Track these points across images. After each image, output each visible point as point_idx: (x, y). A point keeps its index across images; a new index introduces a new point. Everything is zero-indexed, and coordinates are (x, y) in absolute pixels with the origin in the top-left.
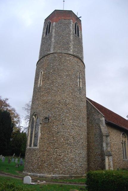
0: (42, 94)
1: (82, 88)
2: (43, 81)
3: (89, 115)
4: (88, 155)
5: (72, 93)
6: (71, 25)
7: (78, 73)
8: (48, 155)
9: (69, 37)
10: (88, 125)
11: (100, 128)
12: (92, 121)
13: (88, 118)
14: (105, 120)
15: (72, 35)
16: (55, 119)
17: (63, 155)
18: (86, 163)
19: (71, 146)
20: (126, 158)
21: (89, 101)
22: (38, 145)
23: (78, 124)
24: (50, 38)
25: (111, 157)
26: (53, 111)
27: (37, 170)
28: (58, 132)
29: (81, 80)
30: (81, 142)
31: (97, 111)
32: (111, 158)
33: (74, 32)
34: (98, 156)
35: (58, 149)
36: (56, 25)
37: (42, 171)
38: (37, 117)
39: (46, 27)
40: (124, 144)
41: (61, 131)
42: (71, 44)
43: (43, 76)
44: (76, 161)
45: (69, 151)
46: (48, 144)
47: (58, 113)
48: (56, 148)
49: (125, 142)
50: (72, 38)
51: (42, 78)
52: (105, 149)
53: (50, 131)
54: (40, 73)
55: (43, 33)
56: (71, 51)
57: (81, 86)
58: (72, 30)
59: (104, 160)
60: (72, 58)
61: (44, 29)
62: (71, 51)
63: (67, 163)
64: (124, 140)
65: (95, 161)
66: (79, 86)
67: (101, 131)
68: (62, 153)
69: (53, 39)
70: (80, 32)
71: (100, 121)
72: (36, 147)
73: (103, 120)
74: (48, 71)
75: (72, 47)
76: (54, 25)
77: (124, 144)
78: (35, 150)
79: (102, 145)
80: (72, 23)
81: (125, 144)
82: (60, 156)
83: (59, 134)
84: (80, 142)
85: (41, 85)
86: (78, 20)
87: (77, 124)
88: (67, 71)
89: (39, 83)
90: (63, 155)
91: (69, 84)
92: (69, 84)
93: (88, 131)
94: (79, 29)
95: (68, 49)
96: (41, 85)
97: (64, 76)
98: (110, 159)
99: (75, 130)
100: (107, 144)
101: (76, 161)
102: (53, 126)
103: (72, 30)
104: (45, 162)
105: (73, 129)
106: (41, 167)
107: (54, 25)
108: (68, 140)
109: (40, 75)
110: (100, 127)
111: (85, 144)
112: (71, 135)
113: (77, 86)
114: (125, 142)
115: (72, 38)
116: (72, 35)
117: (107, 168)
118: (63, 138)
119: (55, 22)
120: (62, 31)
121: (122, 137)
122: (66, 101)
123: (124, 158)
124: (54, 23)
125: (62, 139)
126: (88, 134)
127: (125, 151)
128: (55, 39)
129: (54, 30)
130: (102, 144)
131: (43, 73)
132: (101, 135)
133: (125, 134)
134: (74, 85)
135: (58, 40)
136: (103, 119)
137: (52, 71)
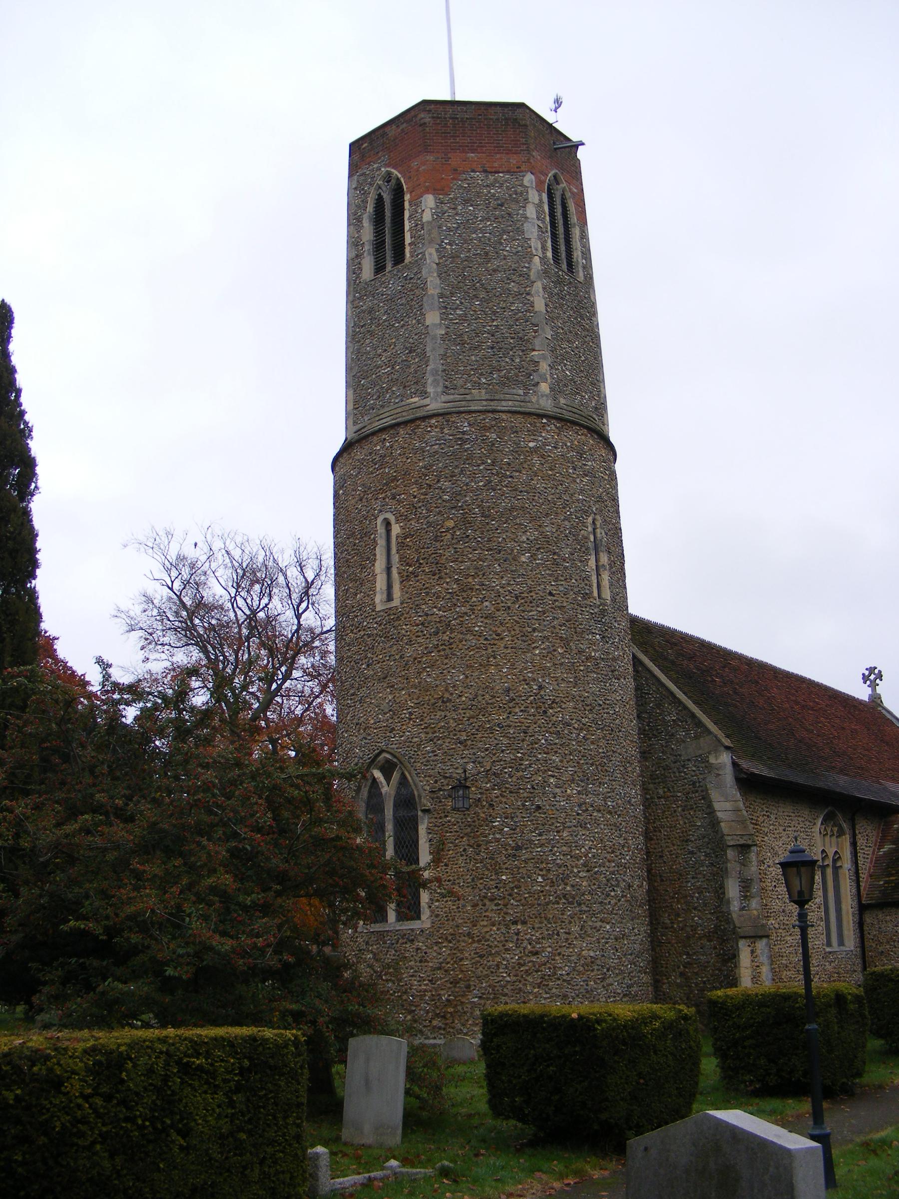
0: (409, 652)
1: (614, 600)
2: (588, 578)
3: (665, 781)
4: (655, 942)
5: (566, 642)
6: (531, 212)
7: (590, 520)
8: (481, 956)
9: (524, 295)
10: (645, 790)
11: (710, 806)
12: (667, 768)
13: (645, 755)
14: (735, 764)
15: (538, 286)
16: (499, 786)
17: (549, 949)
18: (646, 978)
19: (580, 904)
20: (841, 943)
21: (645, 633)
22: (425, 914)
23: (605, 799)
24: (412, 300)
25: (764, 941)
26: (480, 745)
27: (435, 1023)
28: (518, 848)
29: (604, 559)
30: (623, 884)
31: (693, 716)
32: (761, 945)
33: (549, 254)
34: (704, 941)
35: (524, 923)
36: (438, 215)
37: (459, 1026)
38: (396, 776)
39: (370, 208)
40: (829, 871)
41: (531, 841)
42: (537, 342)
43: (401, 545)
44: (608, 970)
45: (575, 929)
46: (475, 906)
47: (508, 757)
48: (515, 923)
49: (835, 861)
50: (540, 304)
51: (395, 558)
52: (735, 906)
53: (479, 846)
54: (381, 529)
55: (354, 243)
56: (544, 387)
57: (607, 594)
58: (535, 244)
59: (731, 958)
60: (549, 433)
61: (354, 220)
62: (544, 387)
63: (568, 982)
64: (831, 852)
65: (687, 965)
66: (595, 594)
67: (715, 823)
68: (546, 943)
69: (432, 318)
70: (576, 232)
71: (709, 767)
72: (415, 925)
73: (721, 767)
74: (429, 524)
75: (544, 367)
76: (427, 217)
77: (829, 871)
78: (410, 938)
79: (720, 893)
80: (533, 196)
81: (836, 869)
82: (537, 953)
83: (524, 854)
84: (617, 886)
85: (396, 602)
86: (561, 153)
87: (599, 802)
88: (533, 519)
89: (381, 583)
90: (549, 949)
91: (551, 594)
92: (551, 594)
93: (647, 821)
94: (574, 219)
95: (526, 377)
96: (396, 602)
97: (522, 552)
98: (759, 952)
99: (587, 822)
100: (746, 885)
101: (608, 970)
102: (489, 820)
103: (535, 244)
104: (468, 987)
105: (583, 826)
106: (451, 1010)
107: (427, 217)
108: (564, 880)
109: (381, 542)
110: (706, 798)
111: (641, 889)
112: (578, 858)
113: (587, 596)
114: (837, 857)
115: (540, 304)
116: (538, 286)
117: (746, 981)
118: (544, 872)
119: (435, 191)
120: (466, 228)
121: (818, 838)
122: (541, 688)
123: (829, 944)
124: (429, 201)
125: (540, 879)
126: (648, 838)
127: (839, 910)
128: (444, 316)
129: (431, 254)
130: (722, 887)
131: (396, 529)
132: (716, 843)
133: (840, 816)
134: (572, 595)
135: (463, 318)
136: (725, 758)
137: (450, 524)
